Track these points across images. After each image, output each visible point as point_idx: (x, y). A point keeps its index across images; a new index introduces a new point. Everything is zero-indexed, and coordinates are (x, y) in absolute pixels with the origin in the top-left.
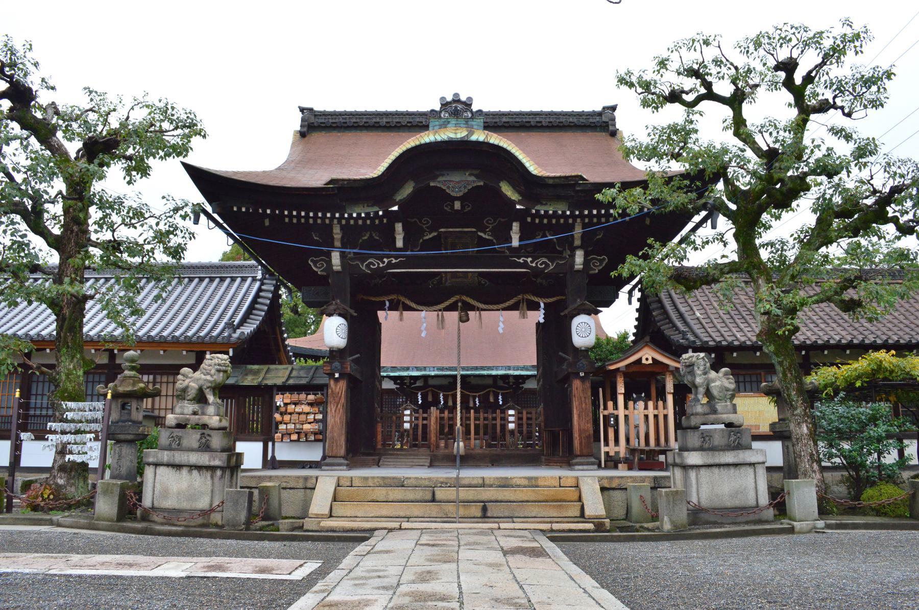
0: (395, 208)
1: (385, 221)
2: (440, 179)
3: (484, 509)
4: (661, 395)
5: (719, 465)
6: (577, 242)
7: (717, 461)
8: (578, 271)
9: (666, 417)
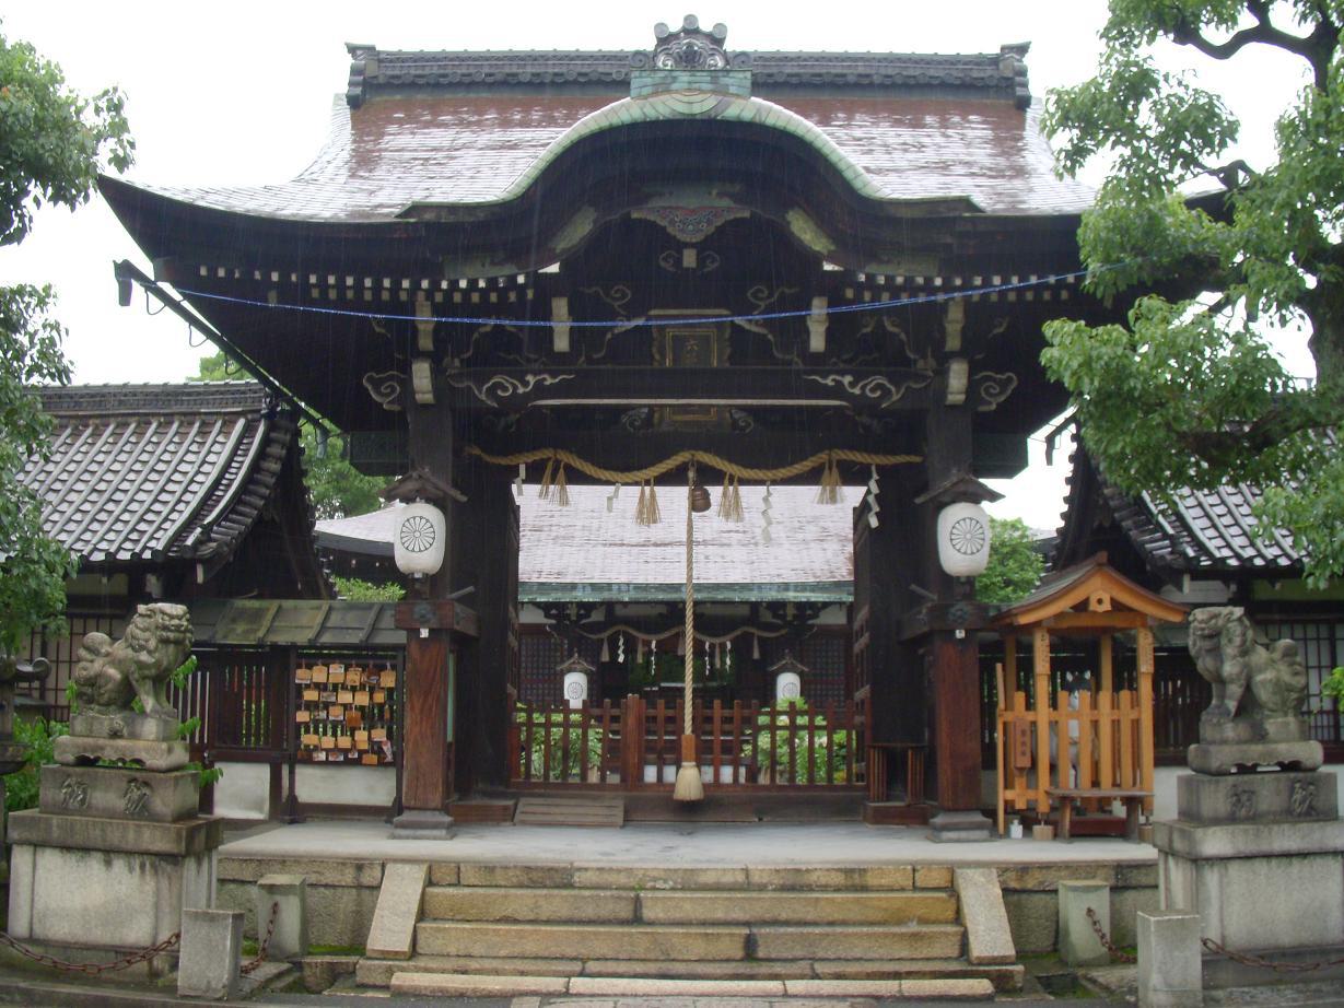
0: (554, 268)
1: (530, 294)
2: (656, 203)
3: (750, 944)
4: (1125, 676)
5: (1268, 856)
6: (953, 343)
7: (1265, 847)
8: (954, 407)
9: (1136, 724)
